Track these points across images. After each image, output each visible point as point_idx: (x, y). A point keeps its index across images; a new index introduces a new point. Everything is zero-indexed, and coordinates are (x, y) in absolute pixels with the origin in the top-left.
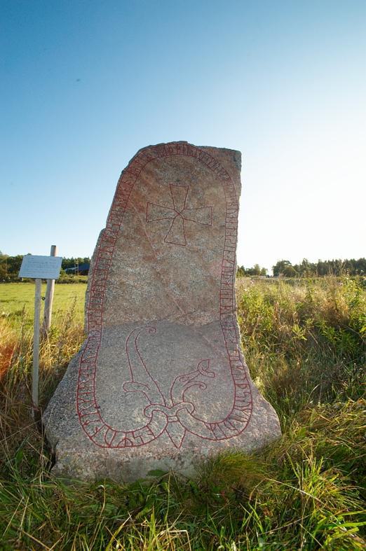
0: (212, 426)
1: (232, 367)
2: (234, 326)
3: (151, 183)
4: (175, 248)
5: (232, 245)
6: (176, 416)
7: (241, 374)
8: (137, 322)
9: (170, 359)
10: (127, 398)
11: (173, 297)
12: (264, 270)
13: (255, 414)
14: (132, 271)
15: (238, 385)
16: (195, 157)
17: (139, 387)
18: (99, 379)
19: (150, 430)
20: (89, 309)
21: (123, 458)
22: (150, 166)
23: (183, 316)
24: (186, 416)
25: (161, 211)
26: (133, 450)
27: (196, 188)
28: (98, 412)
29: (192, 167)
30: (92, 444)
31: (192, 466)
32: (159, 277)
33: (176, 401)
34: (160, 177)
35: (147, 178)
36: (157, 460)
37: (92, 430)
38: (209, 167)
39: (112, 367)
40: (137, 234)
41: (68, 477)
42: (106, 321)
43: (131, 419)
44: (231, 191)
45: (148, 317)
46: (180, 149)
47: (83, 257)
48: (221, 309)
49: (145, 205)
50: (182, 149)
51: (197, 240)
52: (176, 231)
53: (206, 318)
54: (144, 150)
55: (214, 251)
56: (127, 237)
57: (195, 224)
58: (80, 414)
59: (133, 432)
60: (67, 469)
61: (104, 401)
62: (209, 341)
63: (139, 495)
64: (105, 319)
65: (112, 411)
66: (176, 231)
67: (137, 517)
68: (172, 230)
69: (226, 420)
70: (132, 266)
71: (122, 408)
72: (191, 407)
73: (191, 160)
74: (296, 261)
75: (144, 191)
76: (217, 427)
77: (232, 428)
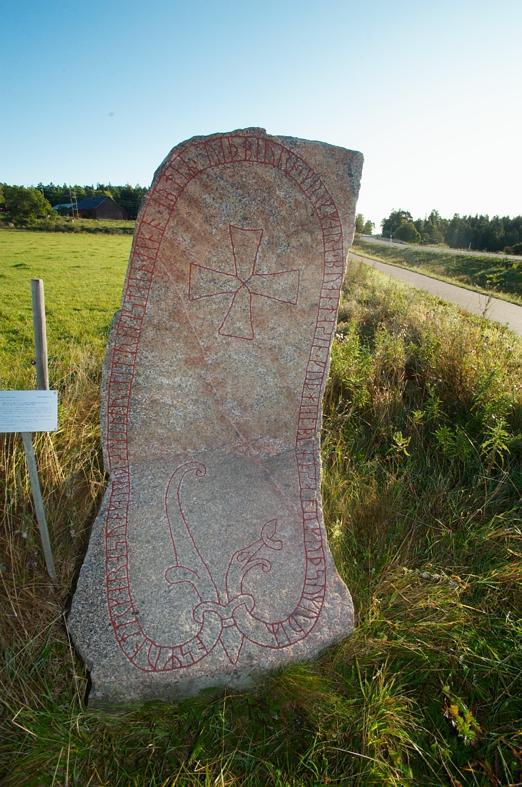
0: (276, 628)
1: (305, 530)
3: (197, 225)
4: (235, 344)
5: (325, 337)
6: (232, 617)
10: (172, 594)
11: (230, 419)
12: (369, 225)
13: (326, 605)
15: (311, 560)
16: (278, 167)
17: (185, 574)
18: (133, 566)
22: (193, 188)
24: (244, 616)
26: (182, 671)
28: (137, 620)
29: (270, 190)
30: (134, 669)
34: (212, 212)
35: (189, 214)
37: (132, 648)
38: (302, 191)
39: (148, 542)
40: (174, 320)
41: (109, 704)
43: (177, 629)
44: (336, 238)
46: (250, 149)
47: (82, 185)
49: (186, 270)
50: (254, 147)
51: (273, 329)
52: (238, 315)
54: (181, 149)
56: (157, 327)
57: (269, 302)
58: (114, 623)
59: (181, 646)
60: (108, 696)
61: (143, 602)
63: (195, 718)
64: (132, 453)
65: (154, 615)
66: (238, 315)
67: (190, 763)
68: (232, 313)
70: (168, 375)
73: (270, 174)
74: (420, 214)
75: (184, 239)
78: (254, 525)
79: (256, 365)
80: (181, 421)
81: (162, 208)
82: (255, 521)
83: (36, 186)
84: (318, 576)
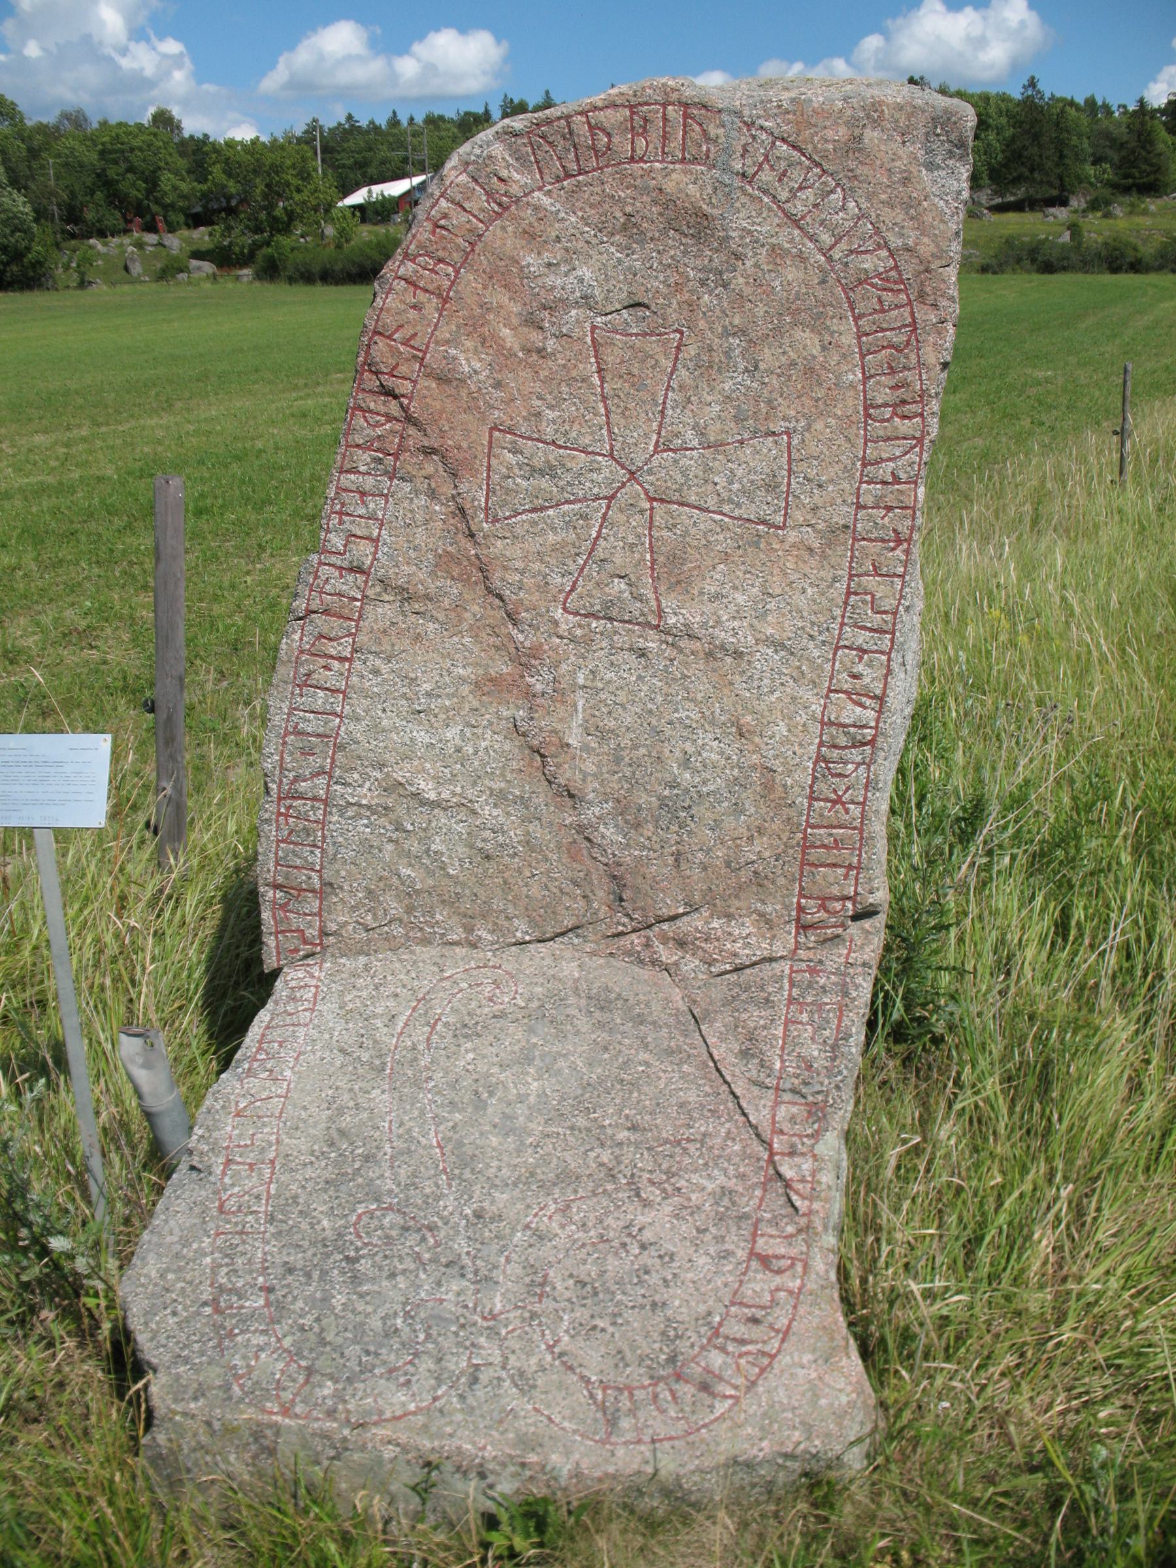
48: (801, 909)
51: (717, 597)
78: (620, 1144)
80: (462, 850)
81: (422, 297)
82: (623, 1135)
83: (299, 131)
84: (774, 1303)
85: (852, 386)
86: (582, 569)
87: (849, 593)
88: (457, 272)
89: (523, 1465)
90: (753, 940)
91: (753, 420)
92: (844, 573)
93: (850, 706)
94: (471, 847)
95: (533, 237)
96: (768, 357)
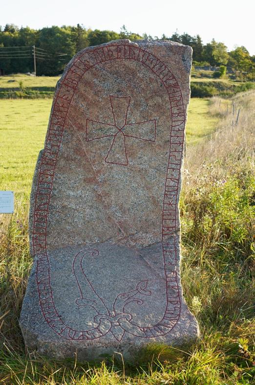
1: (168, 287)
2: (175, 248)
4: (116, 168)
5: (177, 162)
7: (174, 292)
8: (80, 245)
9: (112, 279)
11: (114, 219)
14: (74, 193)
16: (138, 60)
17: (88, 302)
19: (99, 330)
20: (34, 234)
21: (82, 346)
22: (87, 76)
23: (125, 238)
25: (101, 129)
26: (88, 341)
27: (138, 98)
28: (60, 319)
29: (134, 73)
31: (129, 353)
32: (101, 200)
33: (118, 312)
36: (104, 348)
42: (50, 244)
43: (84, 324)
44: (178, 99)
45: (91, 240)
46: (120, 51)
48: (163, 230)
49: (84, 123)
50: (122, 51)
53: (148, 239)
55: (158, 170)
56: (67, 159)
57: (137, 141)
58: (47, 321)
60: (47, 352)
62: (149, 263)
68: (113, 149)
69: (156, 326)
70: (73, 189)
71: (78, 316)
72: (129, 316)
73: (132, 64)
75: (82, 105)
76: (148, 330)
77: (160, 331)
78: (132, 282)
79: (131, 182)
80: (82, 221)
81: (69, 88)
84: (175, 310)
85: (168, 109)
86: (109, 152)
87: (170, 156)
88: (78, 83)
89: (130, 344)
90: (152, 238)
91: (146, 118)
92: (168, 151)
93: (172, 182)
94: (84, 220)
95: (95, 75)
96: (150, 103)
